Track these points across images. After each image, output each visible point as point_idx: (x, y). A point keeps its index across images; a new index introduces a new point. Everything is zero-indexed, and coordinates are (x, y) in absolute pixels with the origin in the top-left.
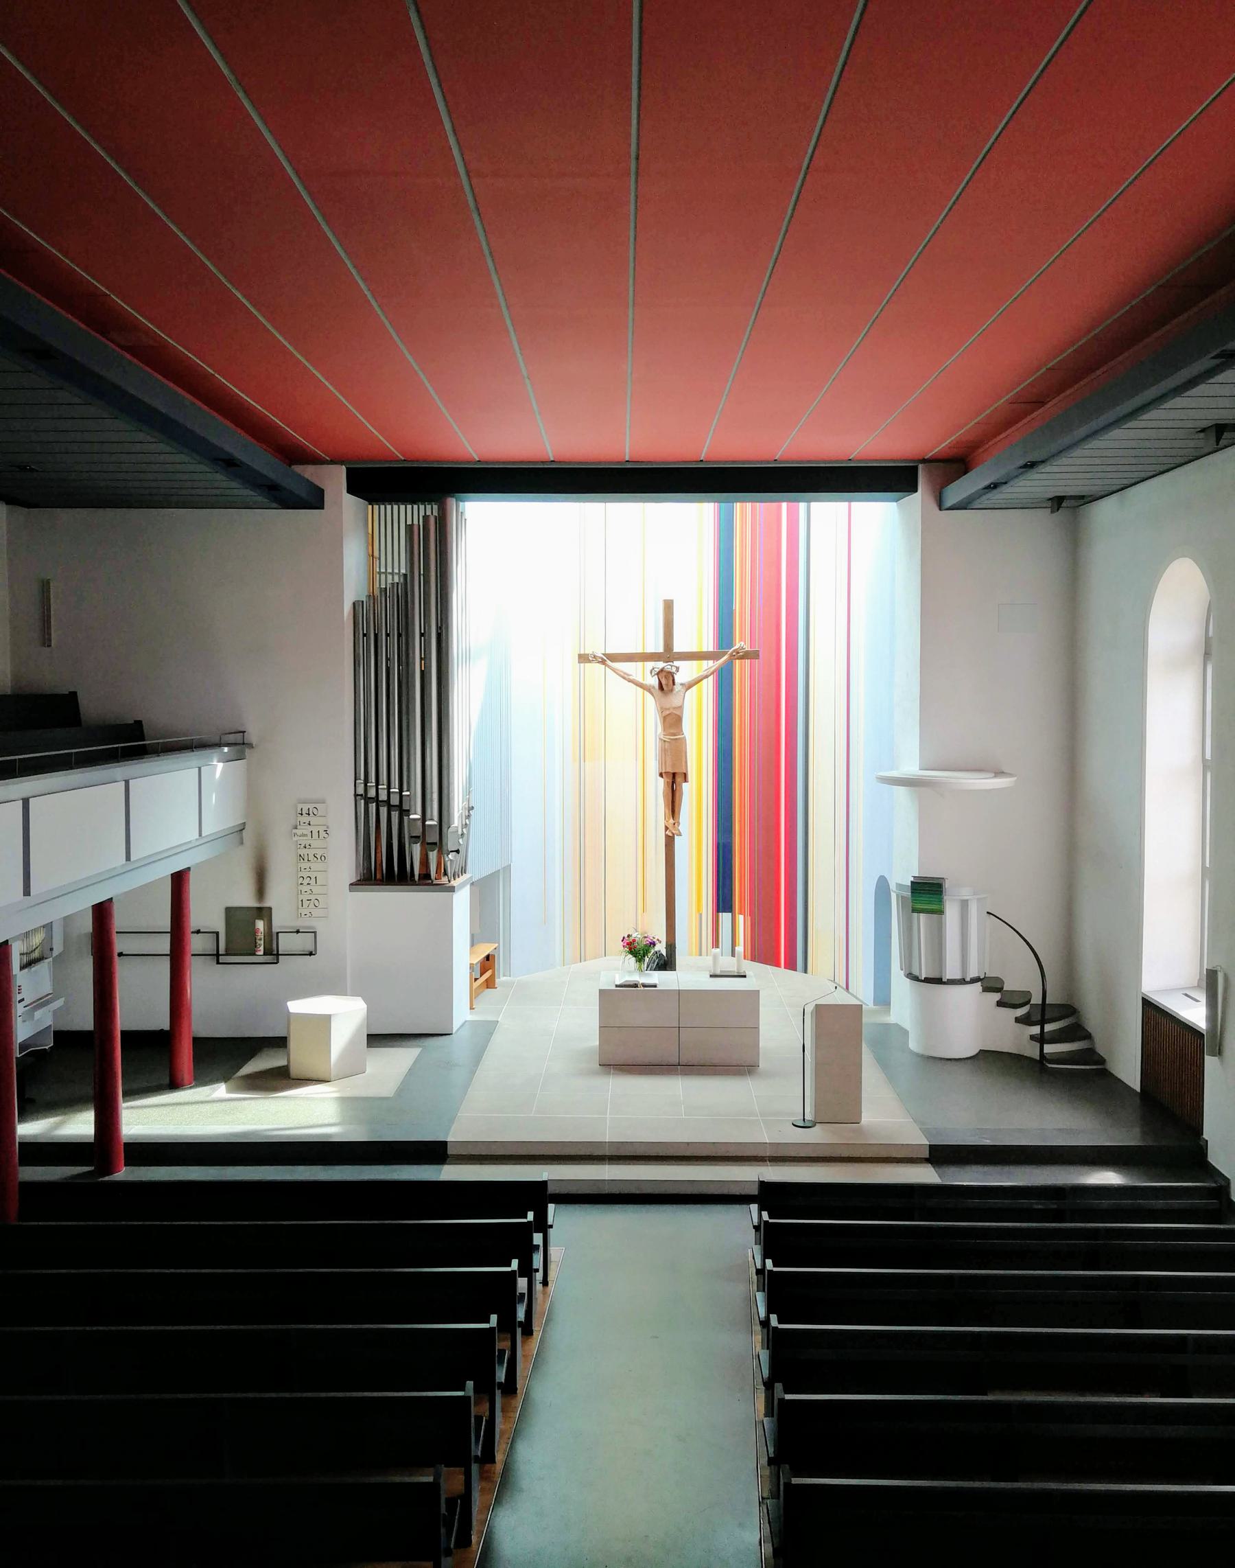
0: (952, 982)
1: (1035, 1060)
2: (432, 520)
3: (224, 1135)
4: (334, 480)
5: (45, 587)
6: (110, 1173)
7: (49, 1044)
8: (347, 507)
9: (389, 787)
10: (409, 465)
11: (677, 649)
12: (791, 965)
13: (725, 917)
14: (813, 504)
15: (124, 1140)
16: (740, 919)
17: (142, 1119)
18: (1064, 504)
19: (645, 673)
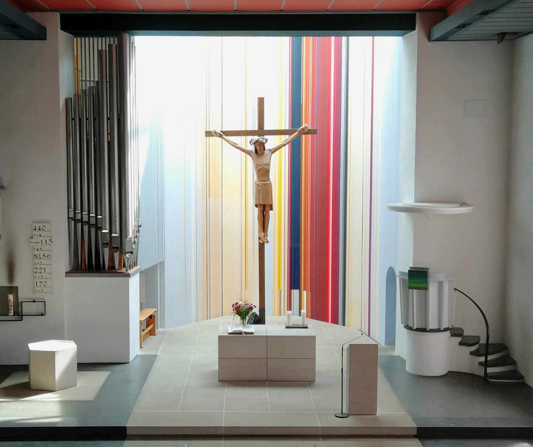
1: (479, 377)
2: (114, 48)
4: (53, 22)
8: (61, 38)
12: (335, 321)
13: (295, 293)
14: (351, 38)
16: (304, 293)
19: (246, 142)
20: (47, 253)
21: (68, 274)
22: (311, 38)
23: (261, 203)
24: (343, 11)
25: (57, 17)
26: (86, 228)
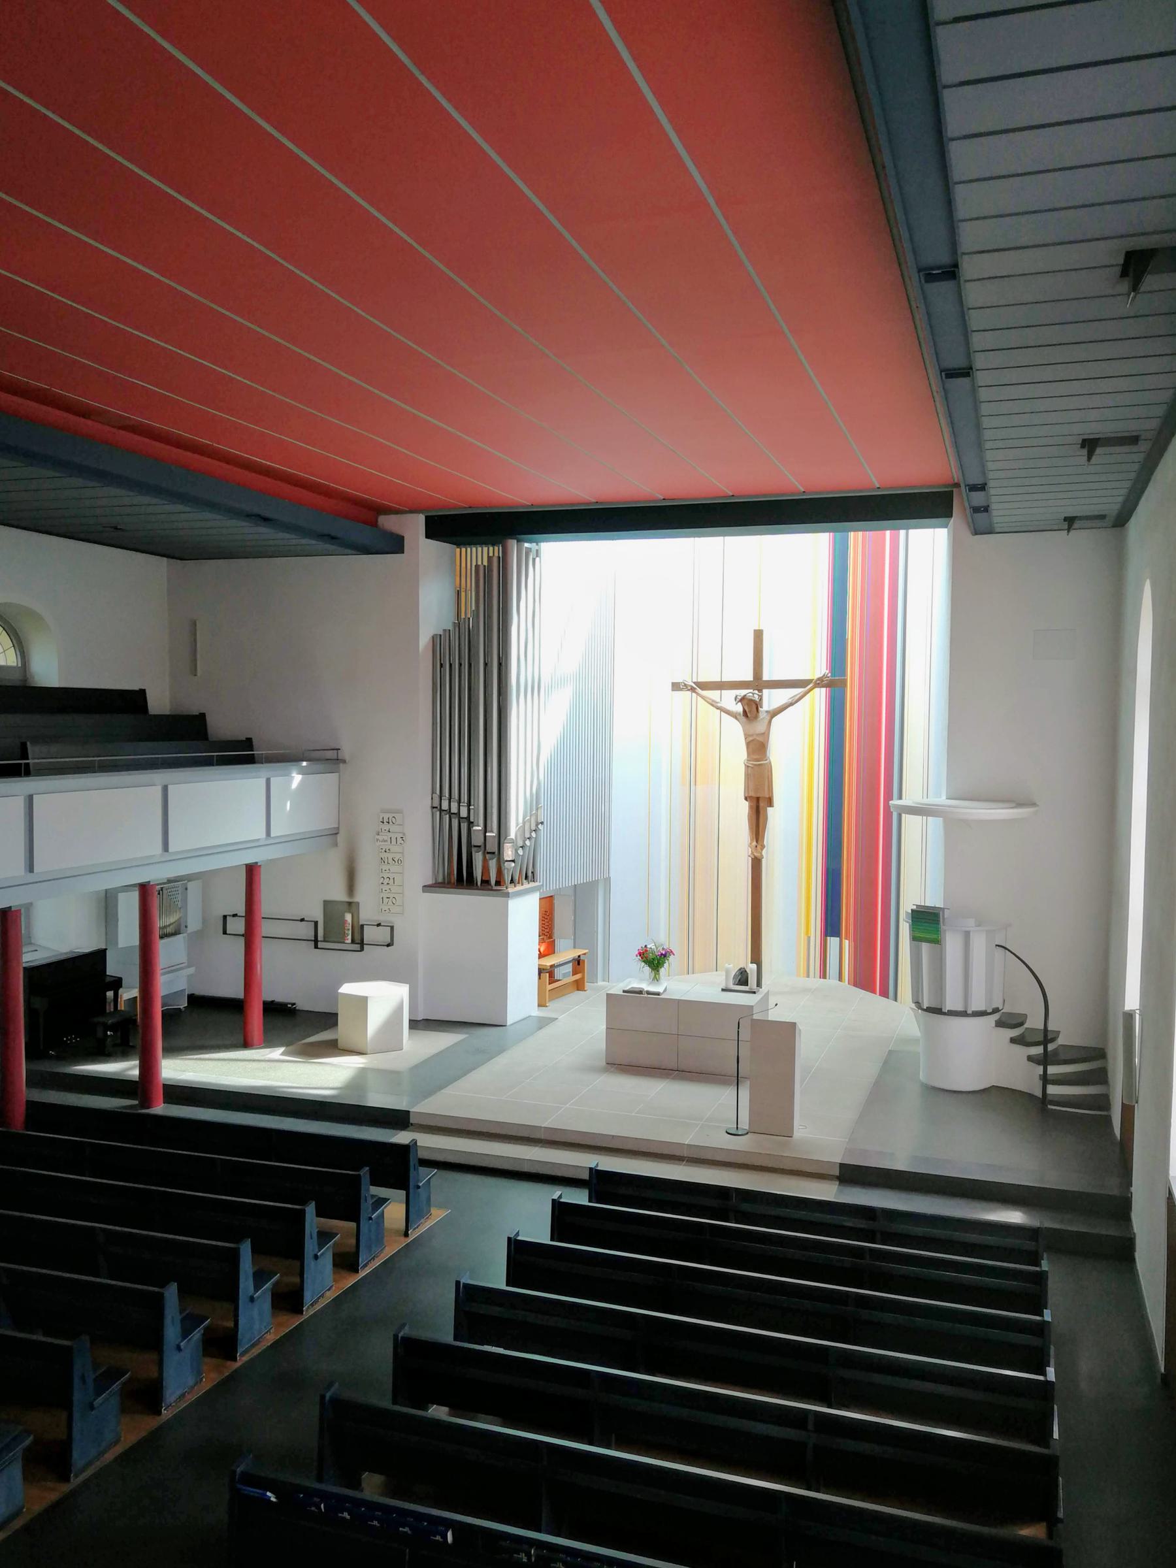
0: (952, 1013)
1: (1031, 1096)
2: (495, 560)
3: (245, 1087)
4: (413, 527)
5: (194, 624)
6: (148, 1108)
7: (183, 1004)
8: (426, 552)
9: (459, 802)
10: (470, 511)
11: (766, 677)
12: (884, 993)
13: (833, 942)
14: (911, 532)
15: (162, 1082)
16: (846, 943)
17: (176, 1069)
18: (1076, 525)
19: (729, 699)
20: (397, 857)
21: (427, 888)
22: (860, 533)
23: (752, 794)
24: (572, 504)
25: (421, 519)
26: (455, 822)
